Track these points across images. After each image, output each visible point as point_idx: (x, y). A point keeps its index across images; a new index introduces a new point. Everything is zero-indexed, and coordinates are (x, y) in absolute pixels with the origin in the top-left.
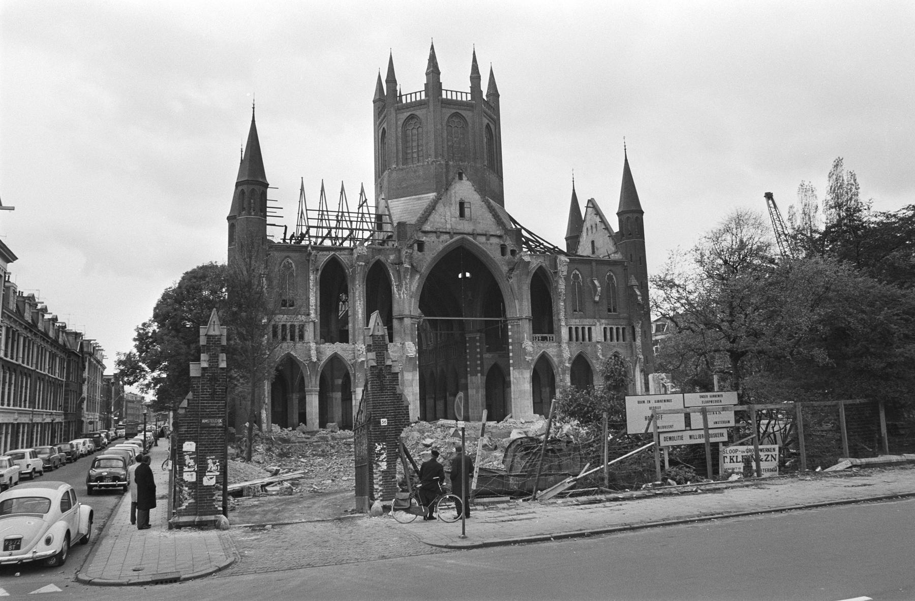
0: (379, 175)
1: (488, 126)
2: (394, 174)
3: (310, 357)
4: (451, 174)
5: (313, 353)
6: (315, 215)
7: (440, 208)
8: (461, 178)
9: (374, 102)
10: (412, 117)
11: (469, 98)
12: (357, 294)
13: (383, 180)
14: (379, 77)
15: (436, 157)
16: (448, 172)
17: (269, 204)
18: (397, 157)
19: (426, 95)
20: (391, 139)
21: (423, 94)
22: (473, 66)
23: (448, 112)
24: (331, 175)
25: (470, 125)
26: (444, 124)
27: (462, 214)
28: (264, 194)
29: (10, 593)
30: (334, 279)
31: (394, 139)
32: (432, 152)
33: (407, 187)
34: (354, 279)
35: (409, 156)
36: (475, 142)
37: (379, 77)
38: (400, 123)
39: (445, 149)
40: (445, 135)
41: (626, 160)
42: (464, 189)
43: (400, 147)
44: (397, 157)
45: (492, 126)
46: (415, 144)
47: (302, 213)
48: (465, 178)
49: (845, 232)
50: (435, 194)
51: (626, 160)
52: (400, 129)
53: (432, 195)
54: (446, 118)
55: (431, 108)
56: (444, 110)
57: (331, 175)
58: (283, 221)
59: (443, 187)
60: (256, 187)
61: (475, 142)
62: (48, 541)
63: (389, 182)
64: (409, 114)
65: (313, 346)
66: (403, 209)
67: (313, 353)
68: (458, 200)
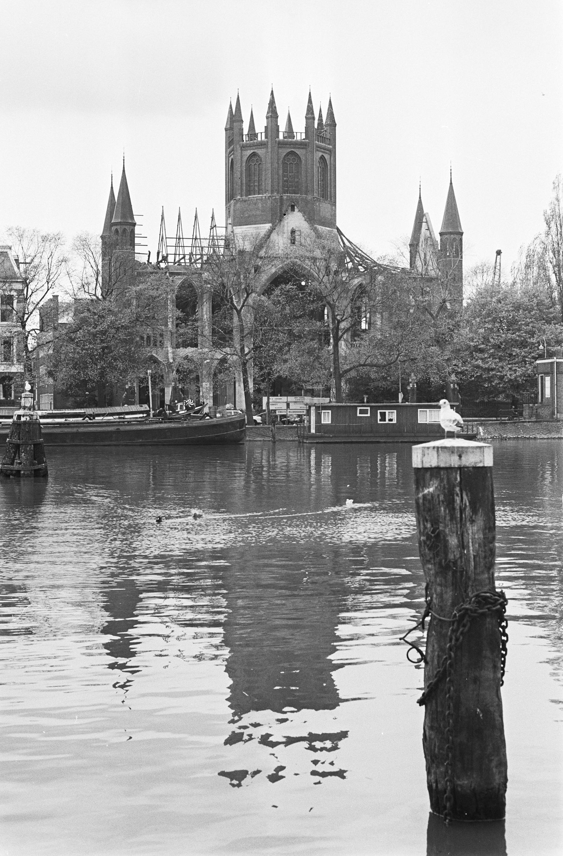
1: (322, 158)
2: (238, 205)
4: (284, 209)
5: (170, 355)
6: (173, 242)
7: (274, 236)
8: (293, 210)
10: (254, 154)
11: (304, 136)
12: (205, 309)
13: (230, 206)
15: (272, 192)
16: (282, 204)
17: (137, 241)
18: (242, 189)
19: (266, 137)
21: (263, 134)
22: (308, 106)
23: (284, 152)
24: (187, 208)
25: (303, 162)
27: (293, 242)
28: (133, 232)
30: (187, 303)
32: (269, 188)
33: (249, 217)
35: (252, 188)
36: (307, 176)
38: (245, 159)
39: (281, 184)
40: (281, 172)
42: (295, 220)
43: (244, 182)
44: (242, 189)
46: (256, 179)
48: (296, 210)
50: (270, 225)
51: (451, 183)
52: (244, 164)
53: (268, 226)
54: (283, 156)
55: (269, 145)
56: (280, 151)
57: (187, 208)
59: (277, 217)
62: (445, 403)
63: (234, 211)
64: (252, 151)
65: (170, 350)
66: (246, 235)
67: (170, 355)
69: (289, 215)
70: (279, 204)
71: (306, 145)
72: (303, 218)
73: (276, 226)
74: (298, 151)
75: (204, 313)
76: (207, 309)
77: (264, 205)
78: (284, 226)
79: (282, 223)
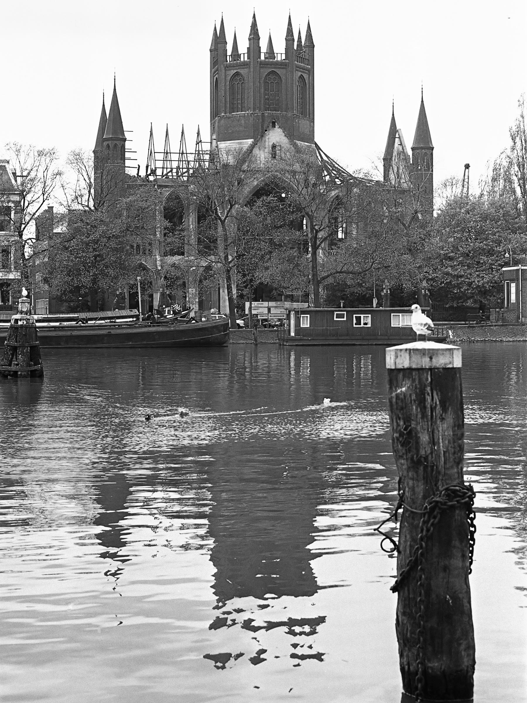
0: (215, 113)
3: (156, 266)
4: (265, 126)
5: (159, 263)
9: (211, 51)
10: (237, 74)
11: (284, 57)
13: (215, 122)
14: (215, 28)
16: (263, 121)
18: (226, 107)
20: (221, 86)
21: (246, 55)
23: (265, 71)
24: (174, 122)
26: (262, 81)
28: (124, 146)
29: (444, 213)
31: (223, 92)
34: (188, 208)
36: (287, 95)
37: (215, 28)
38: (229, 78)
40: (262, 90)
41: (422, 101)
44: (226, 107)
45: (306, 76)
47: (151, 152)
49: (365, 261)
50: (252, 140)
51: (422, 101)
53: (250, 141)
57: (174, 122)
58: (136, 162)
59: (259, 134)
60: (118, 143)
61: (287, 95)
64: (235, 71)
65: (158, 258)
67: (159, 263)
68: (271, 144)
69: (270, 131)
70: (261, 121)
71: (286, 65)
72: (283, 134)
73: (258, 141)
74: (278, 71)
75: (191, 223)
76: (193, 219)
77: (247, 122)
78: (265, 141)
79: (264, 139)
